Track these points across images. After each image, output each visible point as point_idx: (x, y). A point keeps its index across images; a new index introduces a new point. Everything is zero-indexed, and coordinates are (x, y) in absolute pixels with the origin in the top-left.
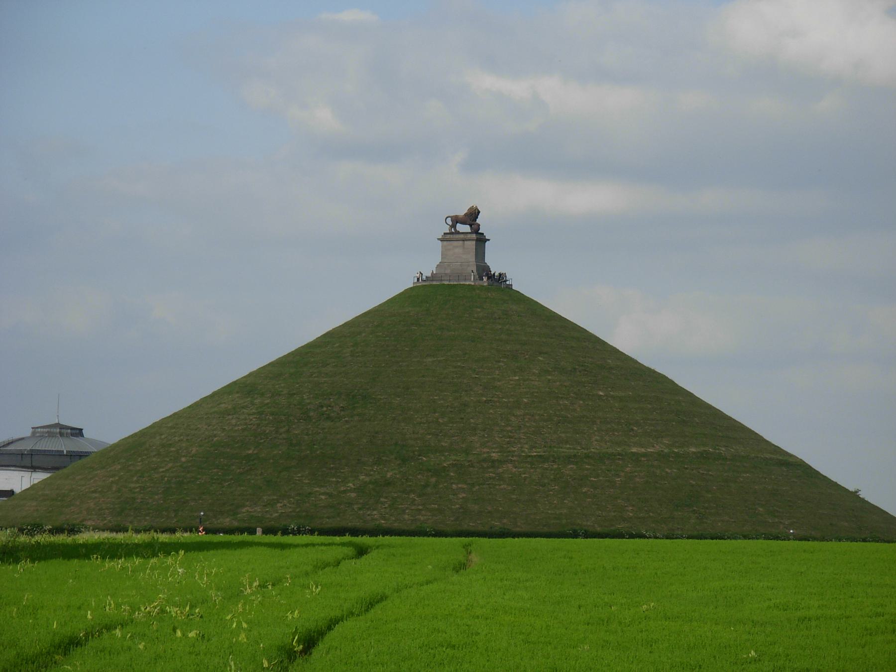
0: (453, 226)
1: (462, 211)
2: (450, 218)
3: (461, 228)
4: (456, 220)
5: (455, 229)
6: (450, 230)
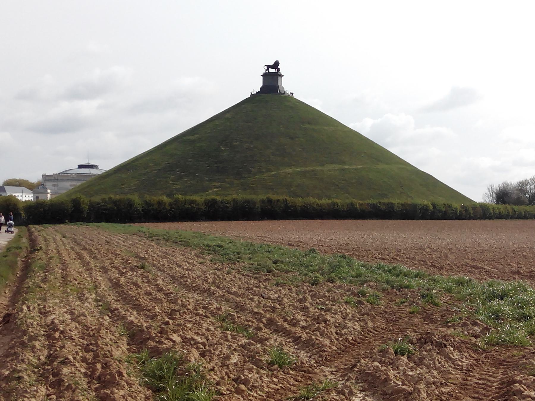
0: (268, 70)
1: (272, 63)
2: (266, 66)
3: (272, 70)
4: (269, 67)
5: (268, 71)
6: (266, 71)
